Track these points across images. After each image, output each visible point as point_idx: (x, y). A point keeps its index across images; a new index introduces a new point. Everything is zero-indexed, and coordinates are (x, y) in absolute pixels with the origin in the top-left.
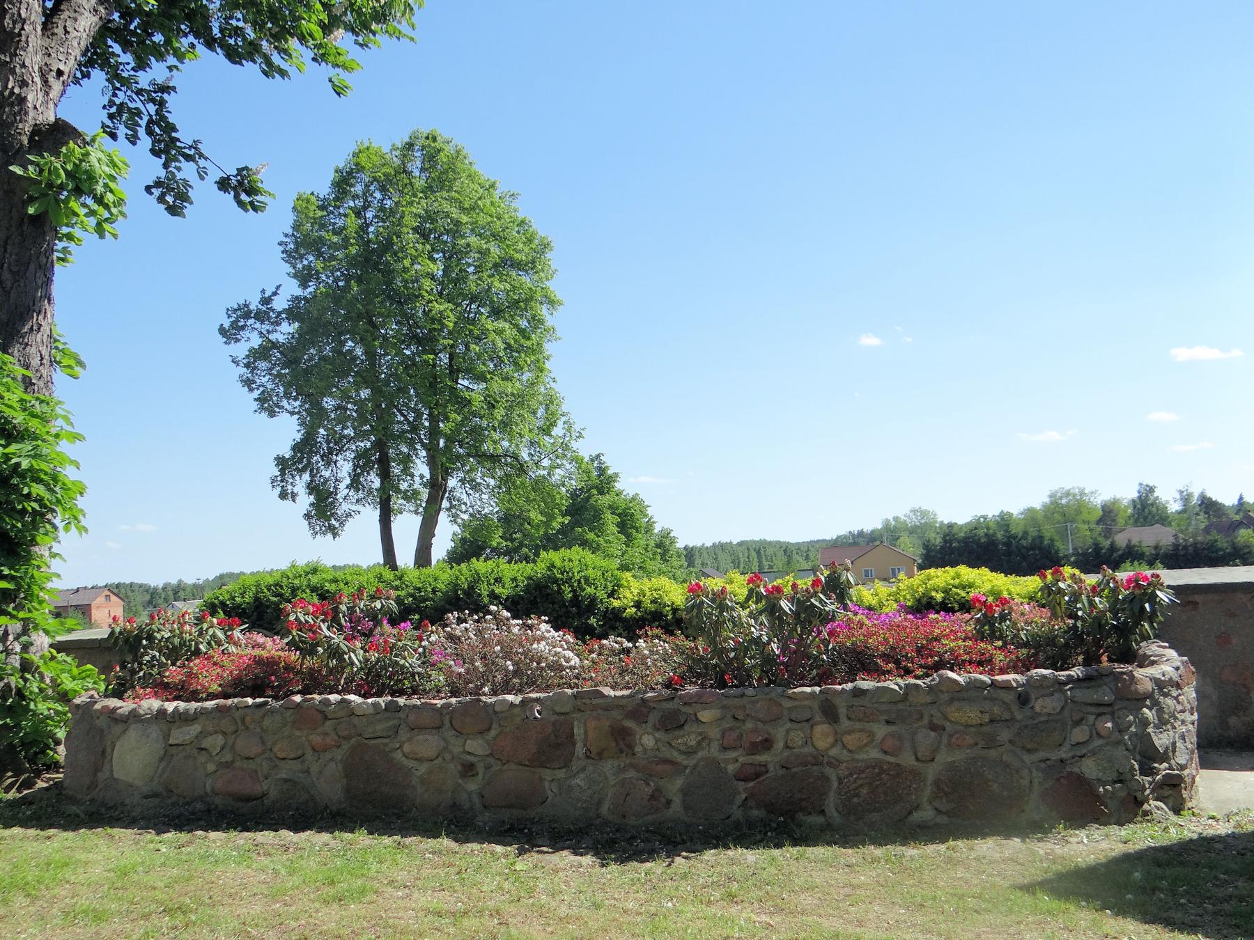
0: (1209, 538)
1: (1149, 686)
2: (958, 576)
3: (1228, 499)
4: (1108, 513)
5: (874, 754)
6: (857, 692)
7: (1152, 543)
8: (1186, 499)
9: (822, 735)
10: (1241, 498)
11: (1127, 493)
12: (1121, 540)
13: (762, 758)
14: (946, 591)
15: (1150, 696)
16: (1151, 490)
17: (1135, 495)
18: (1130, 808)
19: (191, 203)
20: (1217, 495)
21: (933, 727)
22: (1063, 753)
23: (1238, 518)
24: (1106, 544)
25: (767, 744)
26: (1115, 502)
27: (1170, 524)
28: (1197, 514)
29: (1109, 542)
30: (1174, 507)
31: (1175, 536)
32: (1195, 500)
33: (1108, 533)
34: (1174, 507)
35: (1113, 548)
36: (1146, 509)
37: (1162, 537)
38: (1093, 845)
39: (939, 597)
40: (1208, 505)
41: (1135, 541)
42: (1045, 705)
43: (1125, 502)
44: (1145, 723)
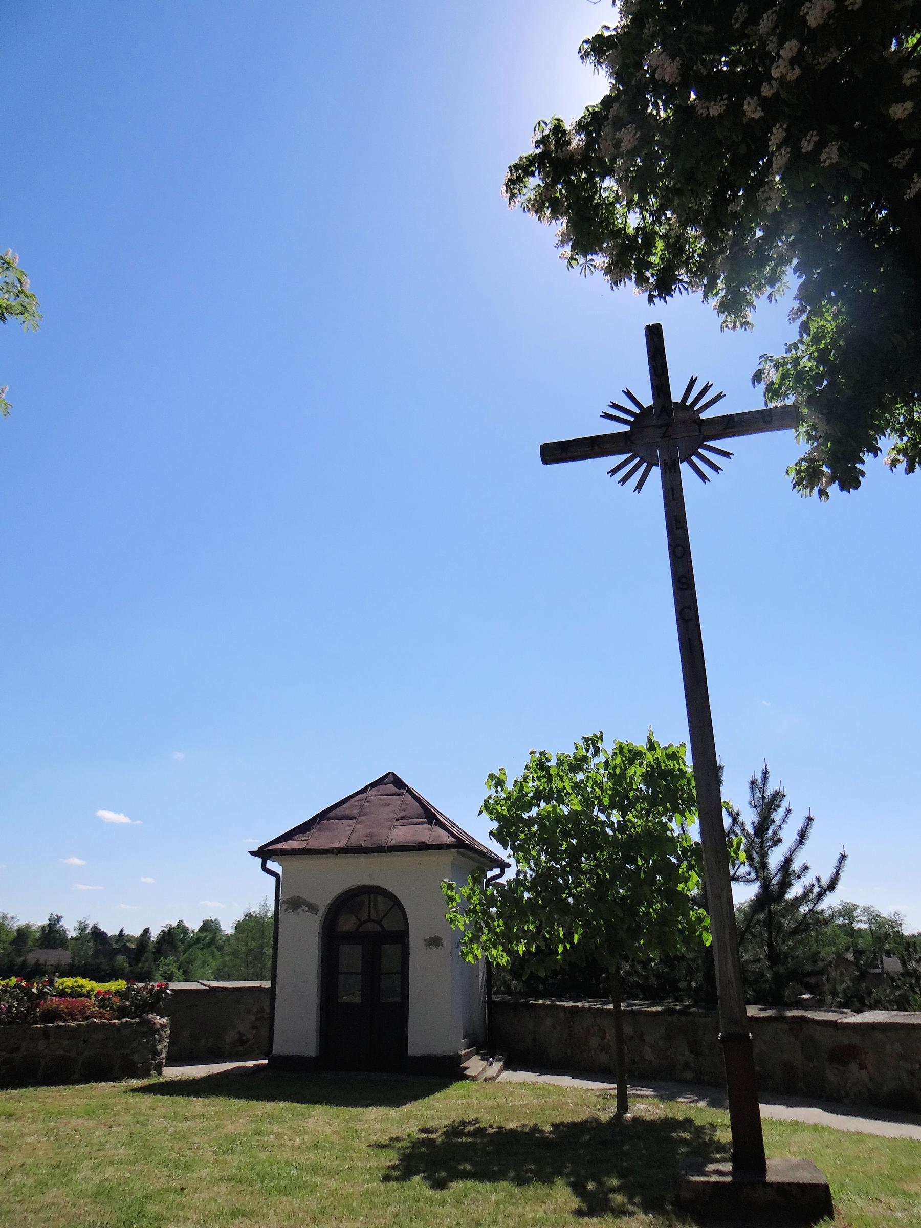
0: (97, 961)
1: (158, 1026)
2: (76, 982)
3: (111, 931)
4: (23, 934)
5: (61, 1052)
6: (59, 1026)
7: (54, 963)
8: (82, 929)
9: (41, 1045)
10: (121, 931)
11: (39, 920)
12: (31, 958)
13: (15, 1055)
14: (71, 988)
15: (158, 1030)
16: (59, 919)
17: (45, 922)
18: (146, 1074)
19: (146, 931)
20: (103, 927)
21: (85, 1041)
22: (128, 1051)
23: (117, 946)
24: (20, 960)
25: (18, 1049)
26: (28, 926)
27: (67, 948)
28: (89, 941)
29: (21, 959)
30: (72, 933)
31: (73, 958)
32: (88, 931)
33: (19, 953)
34: (72, 933)
35: (24, 964)
36: (52, 934)
37: (63, 957)
38: (135, 1083)
39: (69, 991)
40: (97, 934)
41: (42, 961)
42: (127, 1032)
43: (35, 927)
44: (155, 1040)
